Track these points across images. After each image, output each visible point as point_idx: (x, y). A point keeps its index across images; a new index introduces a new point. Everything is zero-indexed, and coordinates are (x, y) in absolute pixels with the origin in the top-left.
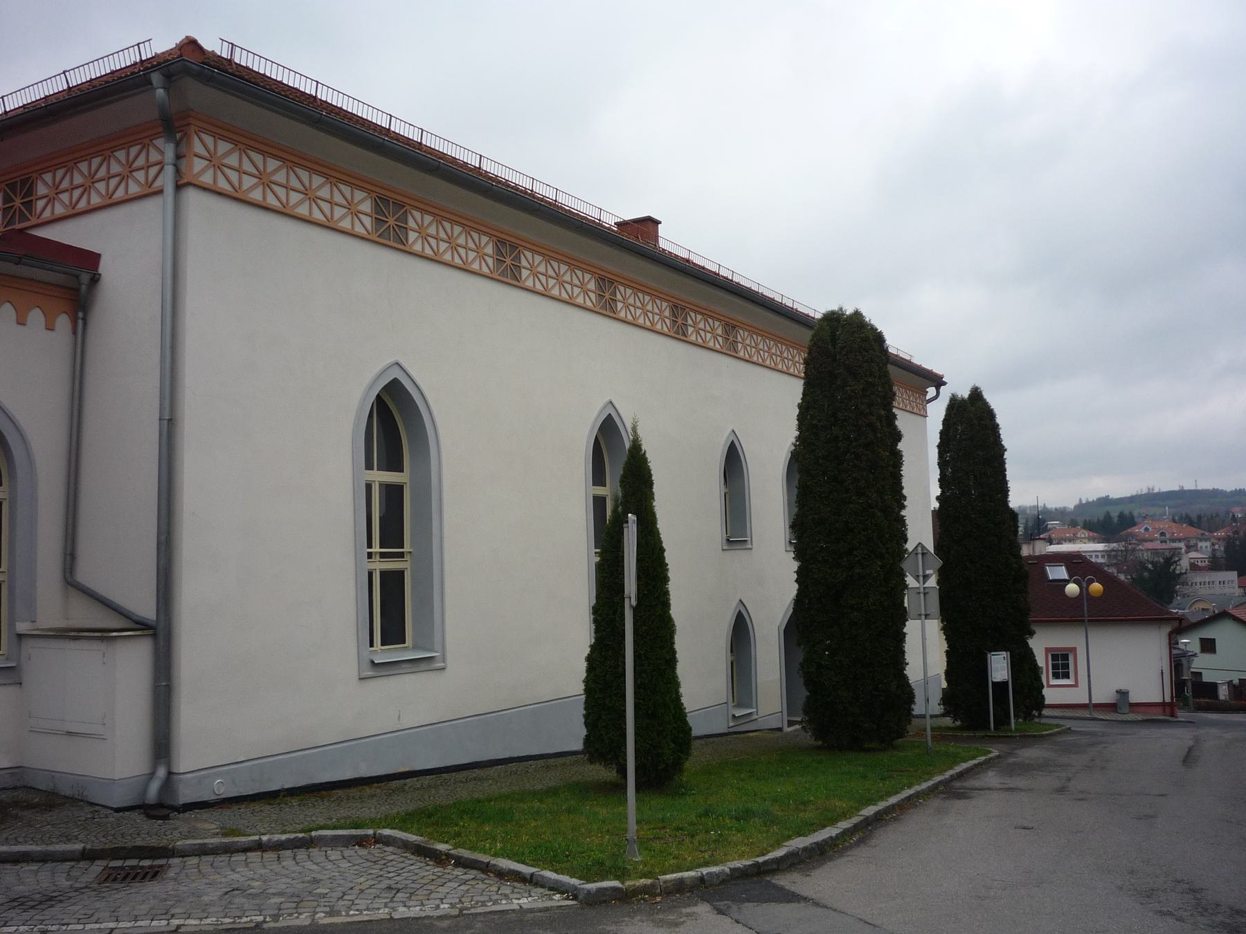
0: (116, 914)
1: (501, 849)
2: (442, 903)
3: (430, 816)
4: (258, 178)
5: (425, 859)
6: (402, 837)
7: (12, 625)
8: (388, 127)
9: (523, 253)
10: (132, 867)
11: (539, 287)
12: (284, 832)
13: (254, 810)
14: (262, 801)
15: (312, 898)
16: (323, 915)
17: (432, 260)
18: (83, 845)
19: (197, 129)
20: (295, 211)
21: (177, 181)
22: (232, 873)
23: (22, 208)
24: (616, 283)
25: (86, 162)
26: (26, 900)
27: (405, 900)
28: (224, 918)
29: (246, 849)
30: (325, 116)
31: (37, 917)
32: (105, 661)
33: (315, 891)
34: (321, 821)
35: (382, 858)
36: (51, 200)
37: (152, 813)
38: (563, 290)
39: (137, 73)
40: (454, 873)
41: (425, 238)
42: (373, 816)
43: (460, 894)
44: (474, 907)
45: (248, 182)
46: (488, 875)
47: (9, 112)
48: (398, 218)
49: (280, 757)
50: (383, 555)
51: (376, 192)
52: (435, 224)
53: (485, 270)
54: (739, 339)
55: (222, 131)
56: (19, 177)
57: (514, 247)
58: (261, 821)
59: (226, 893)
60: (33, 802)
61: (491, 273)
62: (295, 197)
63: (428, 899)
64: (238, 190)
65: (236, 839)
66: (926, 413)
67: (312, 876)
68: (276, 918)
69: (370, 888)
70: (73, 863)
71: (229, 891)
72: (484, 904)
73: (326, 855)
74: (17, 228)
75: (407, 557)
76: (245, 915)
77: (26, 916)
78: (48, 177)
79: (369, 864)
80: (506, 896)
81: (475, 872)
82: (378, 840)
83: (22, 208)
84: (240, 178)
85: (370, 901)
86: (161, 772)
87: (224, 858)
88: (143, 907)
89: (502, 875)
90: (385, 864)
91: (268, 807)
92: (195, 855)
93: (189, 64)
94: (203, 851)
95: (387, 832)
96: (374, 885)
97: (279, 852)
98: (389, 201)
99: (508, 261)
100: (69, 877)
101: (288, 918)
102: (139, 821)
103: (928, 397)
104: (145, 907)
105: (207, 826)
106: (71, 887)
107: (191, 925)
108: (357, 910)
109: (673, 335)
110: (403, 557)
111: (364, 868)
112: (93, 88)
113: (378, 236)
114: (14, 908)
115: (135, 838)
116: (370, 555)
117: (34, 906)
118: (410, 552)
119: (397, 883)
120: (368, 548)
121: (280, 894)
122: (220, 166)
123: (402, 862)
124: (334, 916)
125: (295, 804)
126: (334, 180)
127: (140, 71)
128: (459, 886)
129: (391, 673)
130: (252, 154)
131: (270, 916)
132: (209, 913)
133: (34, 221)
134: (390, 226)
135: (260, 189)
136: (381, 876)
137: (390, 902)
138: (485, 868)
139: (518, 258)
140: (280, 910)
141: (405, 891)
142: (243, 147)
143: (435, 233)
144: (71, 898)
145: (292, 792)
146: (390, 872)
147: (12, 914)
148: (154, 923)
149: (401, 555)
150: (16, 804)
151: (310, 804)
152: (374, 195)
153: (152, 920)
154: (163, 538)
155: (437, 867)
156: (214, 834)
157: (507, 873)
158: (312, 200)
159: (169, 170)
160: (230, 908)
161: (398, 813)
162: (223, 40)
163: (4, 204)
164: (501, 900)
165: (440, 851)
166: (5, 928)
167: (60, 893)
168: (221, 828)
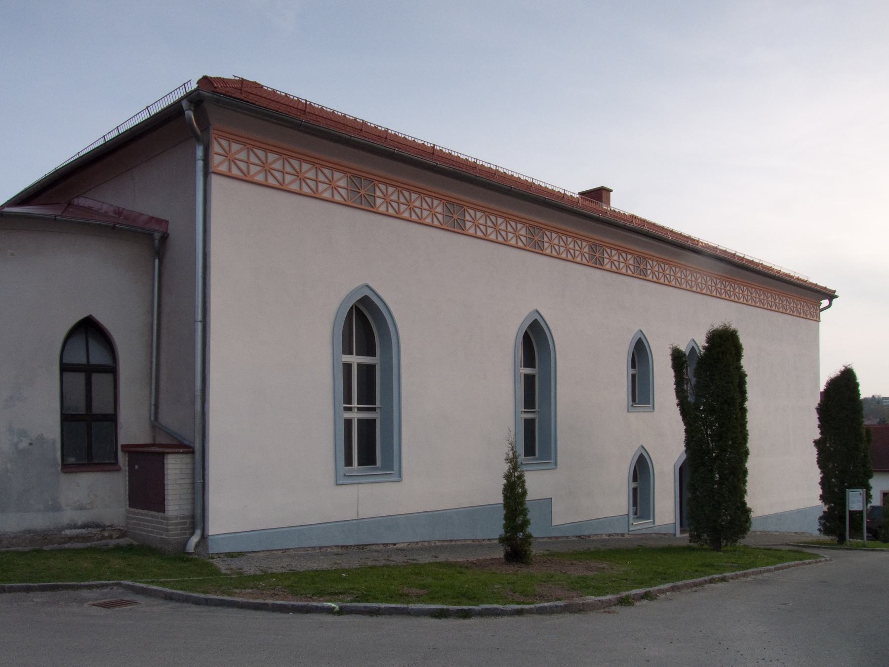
4: (296, 176)
9: (468, 212)
19: (216, 136)
24: (543, 230)
30: (305, 122)
45: (254, 169)
54: (649, 267)
64: (247, 175)
66: (819, 319)
75: (378, 411)
86: (93, 535)
103: (821, 307)
109: (592, 265)
130: (256, 151)
134: (361, 195)
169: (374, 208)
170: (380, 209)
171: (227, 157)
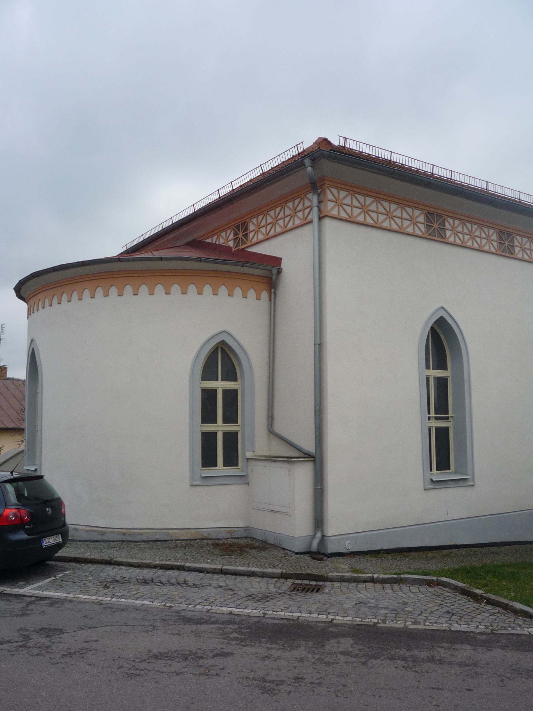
0: (300, 609)
1: (515, 596)
2: (480, 625)
3: (468, 572)
4: (469, 235)
5: (468, 597)
6: (453, 583)
7: (244, 454)
8: (344, 146)
9: (516, 238)
10: (307, 585)
11: (458, 241)
12: (385, 574)
13: (367, 560)
14: (371, 555)
15: (403, 613)
16: (410, 623)
17: (460, 246)
18: (281, 570)
20: (331, 213)
21: (319, 215)
22: (358, 593)
23: (243, 238)
25: (273, 210)
26: (255, 596)
27: (457, 620)
28: (356, 618)
29: (365, 581)
30: (396, 170)
31: (261, 606)
32: (290, 474)
33: (405, 609)
34: (406, 570)
35: (442, 594)
36: (256, 232)
37: (315, 556)
38: (491, 246)
39: (297, 160)
40: (486, 608)
41: (456, 233)
42: (435, 569)
43: (491, 621)
44: (500, 630)
45: (356, 211)
46: (508, 611)
47: (235, 189)
48: (439, 224)
49: (381, 531)
50: (436, 418)
51: (499, 229)
52: (461, 225)
53: (492, 249)
55: (341, 185)
56: (241, 222)
57: (509, 234)
58: (372, 566)
59: (356, 604)
60: (256, 545)
61: (423, 234)
62: (381, 217)
63: (471, 622)
64: (351, 217)
65: (360, 575)
67: (403, 600)
68: (384, 621)
69: (436, 611)
70: (276, 579)
71: (358, 603)
72: (506, 629)
73: (410, 589)
74: (241, 248)
75: (450, 420)
76: (368, 617)
77: (256, 604)
78: (254, 220)
79: (435, 597)
80: (520, 626)
81: (499, 608)
82: (439, 583)
83: (243, 238)
84: (352, 210)
85: (437, 619)
86: (319, 535)
87: (354, 584)
88: (313, 606)
89: (516, 612)
90: (444, 598)
91: (375, 559)
92: (338, 582)
93: (323, 151)
94: (342, 580)
95: (444, 579)
96: (439, 609)
97: (383, 585)
98: (434, 214)
99: (506, 243)
100: (275, 587)
101: (391, 622)
102: (308, 560)
104: (314, 607)
105: (343, 566)
106: (276, 592)
107: (339, 620)
108: (430, 623)
110: (448, 420)
111: (432, 598)
112: (275, 171)
113: (429, 235)
114: (250, 600)
115: (306, 570)
116: (429, 418)
117: (259, 600)
118: (452, 417)
119: (452, 610)
120: (428, 414)
121: (386, 608)
122: (392, 217)
123: (455, 598)
124: (417, 624)
125: (389, 558)
126: (379, 199)
127: (298, 159)
128: (490, 616)
129: (443, 486)
131: (381, 620)
132: (348, 614)
133: (249, 244)
135: (412, 226)
136: (442, 605)
137: (449, 620)
138: (506, 607)
139: (512, 241)
140: (386, 617)
141: (457, 615)
142: (353, 193)
143: (376, 209)
144: (277, 597)
145: (388, 551)
146: (447, 603)
147: (249, 603)
148: (320, 616)
149: (447, 418)
150: (247, 546)
151: (398, 559)
152: (425, 211)
153: (319, 614)
154: (318, 408)
155: (476, 603)
156: (347, 571)
157: (520, 611)
158: (391, 218)
159: (315, 210)
160: (359, 613)
161: (449, 569)
162: (340, 136)
163: (234, 236)
164: (517, 627)
165: (477, 594)
166: (246, 610)
167: (271, 595)
168: (351, 568)
169: (444, 239)
170: (450, 240)
171: (388, 215)
